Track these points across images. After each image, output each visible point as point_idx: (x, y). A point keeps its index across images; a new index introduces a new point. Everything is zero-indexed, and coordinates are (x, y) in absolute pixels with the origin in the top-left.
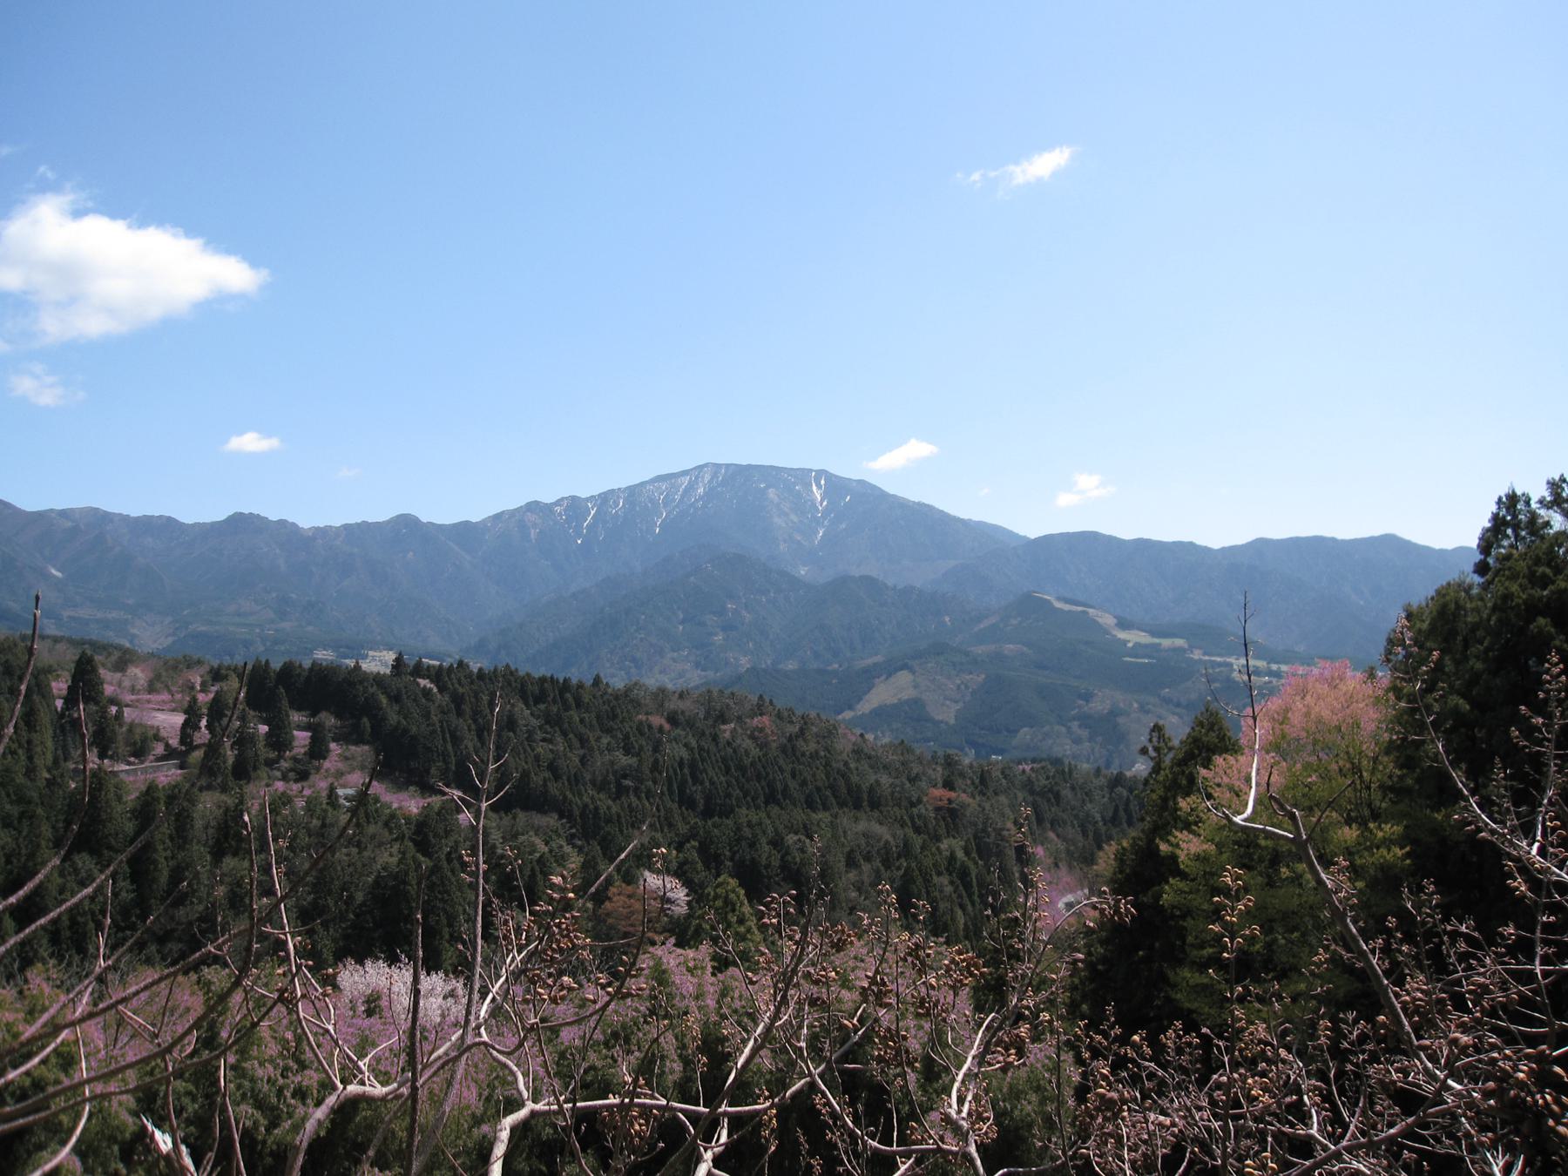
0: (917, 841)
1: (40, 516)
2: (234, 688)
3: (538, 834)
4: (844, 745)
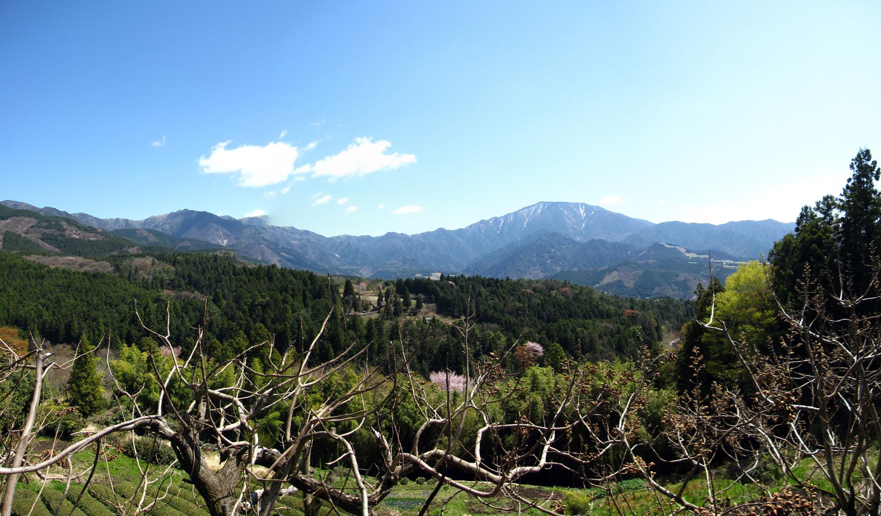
0: (622, 328)
1: (331, 239)
2: (392, 287)
3: (491, 331)
4: (596, 296)
